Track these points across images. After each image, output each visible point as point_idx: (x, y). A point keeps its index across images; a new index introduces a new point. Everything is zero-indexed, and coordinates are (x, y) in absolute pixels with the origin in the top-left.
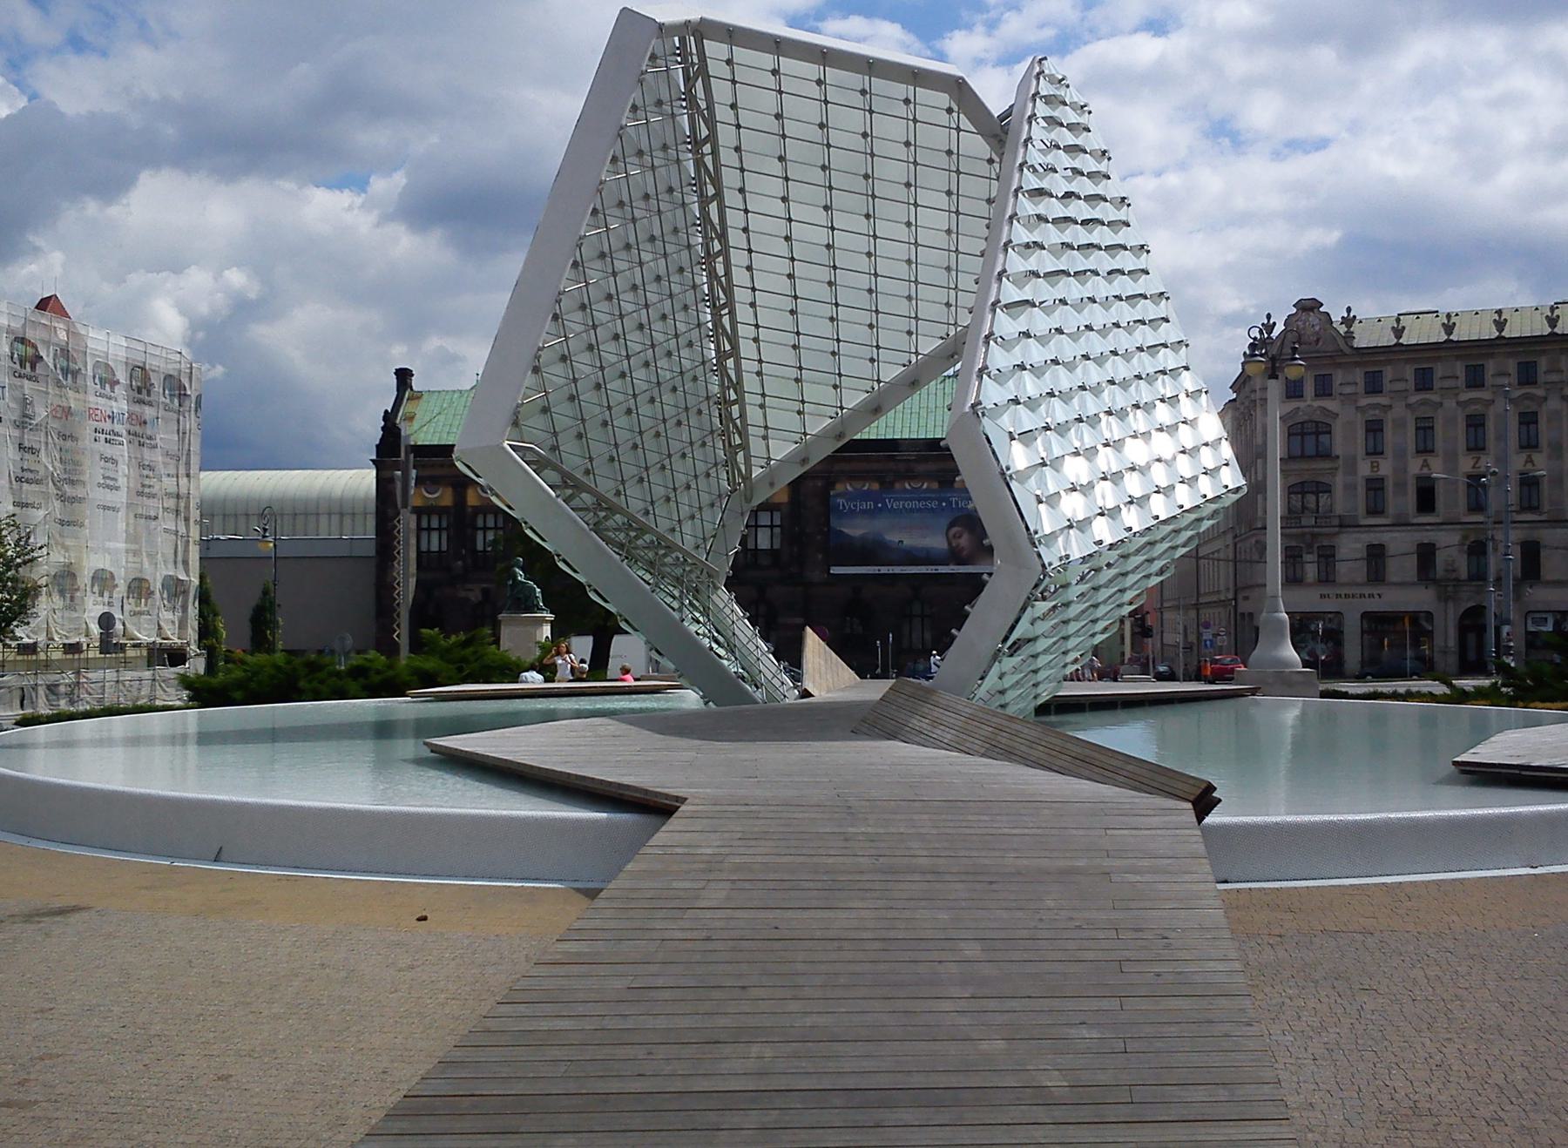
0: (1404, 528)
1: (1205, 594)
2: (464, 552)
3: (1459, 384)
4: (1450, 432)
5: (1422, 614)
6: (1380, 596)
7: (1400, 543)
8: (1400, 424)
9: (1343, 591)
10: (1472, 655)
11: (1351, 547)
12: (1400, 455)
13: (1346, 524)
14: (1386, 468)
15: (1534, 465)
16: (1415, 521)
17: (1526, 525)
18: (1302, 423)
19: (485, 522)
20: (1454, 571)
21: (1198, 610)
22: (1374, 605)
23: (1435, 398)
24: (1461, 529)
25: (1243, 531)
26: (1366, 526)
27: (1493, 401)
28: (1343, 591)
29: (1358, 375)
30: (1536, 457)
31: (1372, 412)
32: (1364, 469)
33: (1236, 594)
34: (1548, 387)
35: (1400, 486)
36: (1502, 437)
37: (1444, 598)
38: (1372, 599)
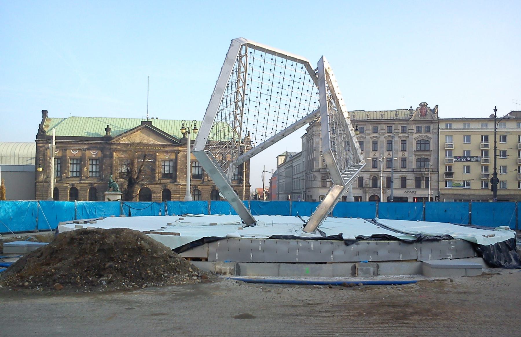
1: (295, 190)
2: (66, 171)
3: (414, 131)
4: (397, 145)
17: (388, 172)
18: (421, 140)
19: (422, 161)
21: (292, 194)
23: (364, 136)
25: (309, 172)
33: (306, 190)
36: (381, 148)
37: (365, 193)
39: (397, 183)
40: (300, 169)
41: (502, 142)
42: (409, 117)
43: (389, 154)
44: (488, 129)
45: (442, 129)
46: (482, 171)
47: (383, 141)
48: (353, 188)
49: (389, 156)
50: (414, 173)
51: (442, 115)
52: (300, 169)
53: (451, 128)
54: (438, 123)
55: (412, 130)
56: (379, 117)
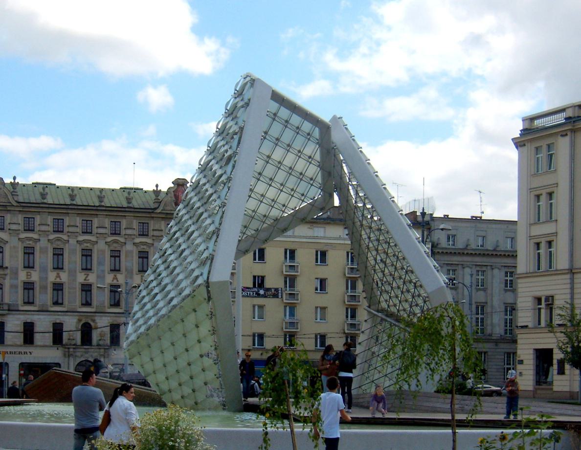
5: (77, 367)
6: (30, 353)
7: (43, 324)
8: (44, 251)
9: (9, 349)
12: (44, 270)
13: (12, 309)
14: (35, 277)
15: (118, 281)
16: (21, 308)
17: (114, 315)
20: (74, 339)
24: (77, 315)
26: (23, 311)
28: (9, 349)
29: (20, 218)
31: (85, 245)
32: (23, 276)
35: (44, 288)
36: (100, 263)
37: (68, 355)
38: (26, 355)
41: (319, 263)
42: (156, 205)
46: (285, 315)
47: (101, 249)
48: (242, 349)
49: (115, 281)
51: (437, 215)
55: (160, 232)
56: (35, 198)
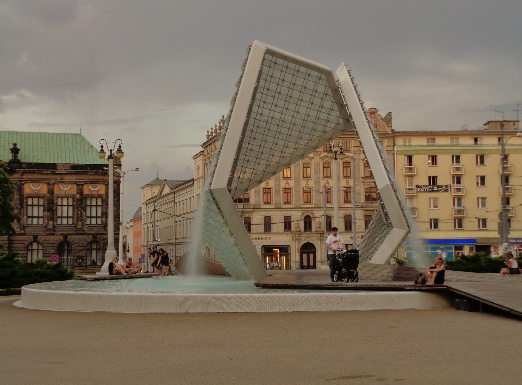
0: (279, 210)
1: (180, 238)
7: (278, 217)
10: (305, 264)
11: (257, 218)
13: (255, 208)
15: (329, 185)
22: (268, 243)
24: (301, 210)
27: (314, 158)
30: (330, 181)
34: (355, 152)
39: (278, 227)
40: (190, 207)
43: (287, 183)
44: (413, 146)
45: (399, 146)
49: (287, 186)
50: (363, 210)
52: (190, 207)
53: (434, 145)
54: (394, 137)
